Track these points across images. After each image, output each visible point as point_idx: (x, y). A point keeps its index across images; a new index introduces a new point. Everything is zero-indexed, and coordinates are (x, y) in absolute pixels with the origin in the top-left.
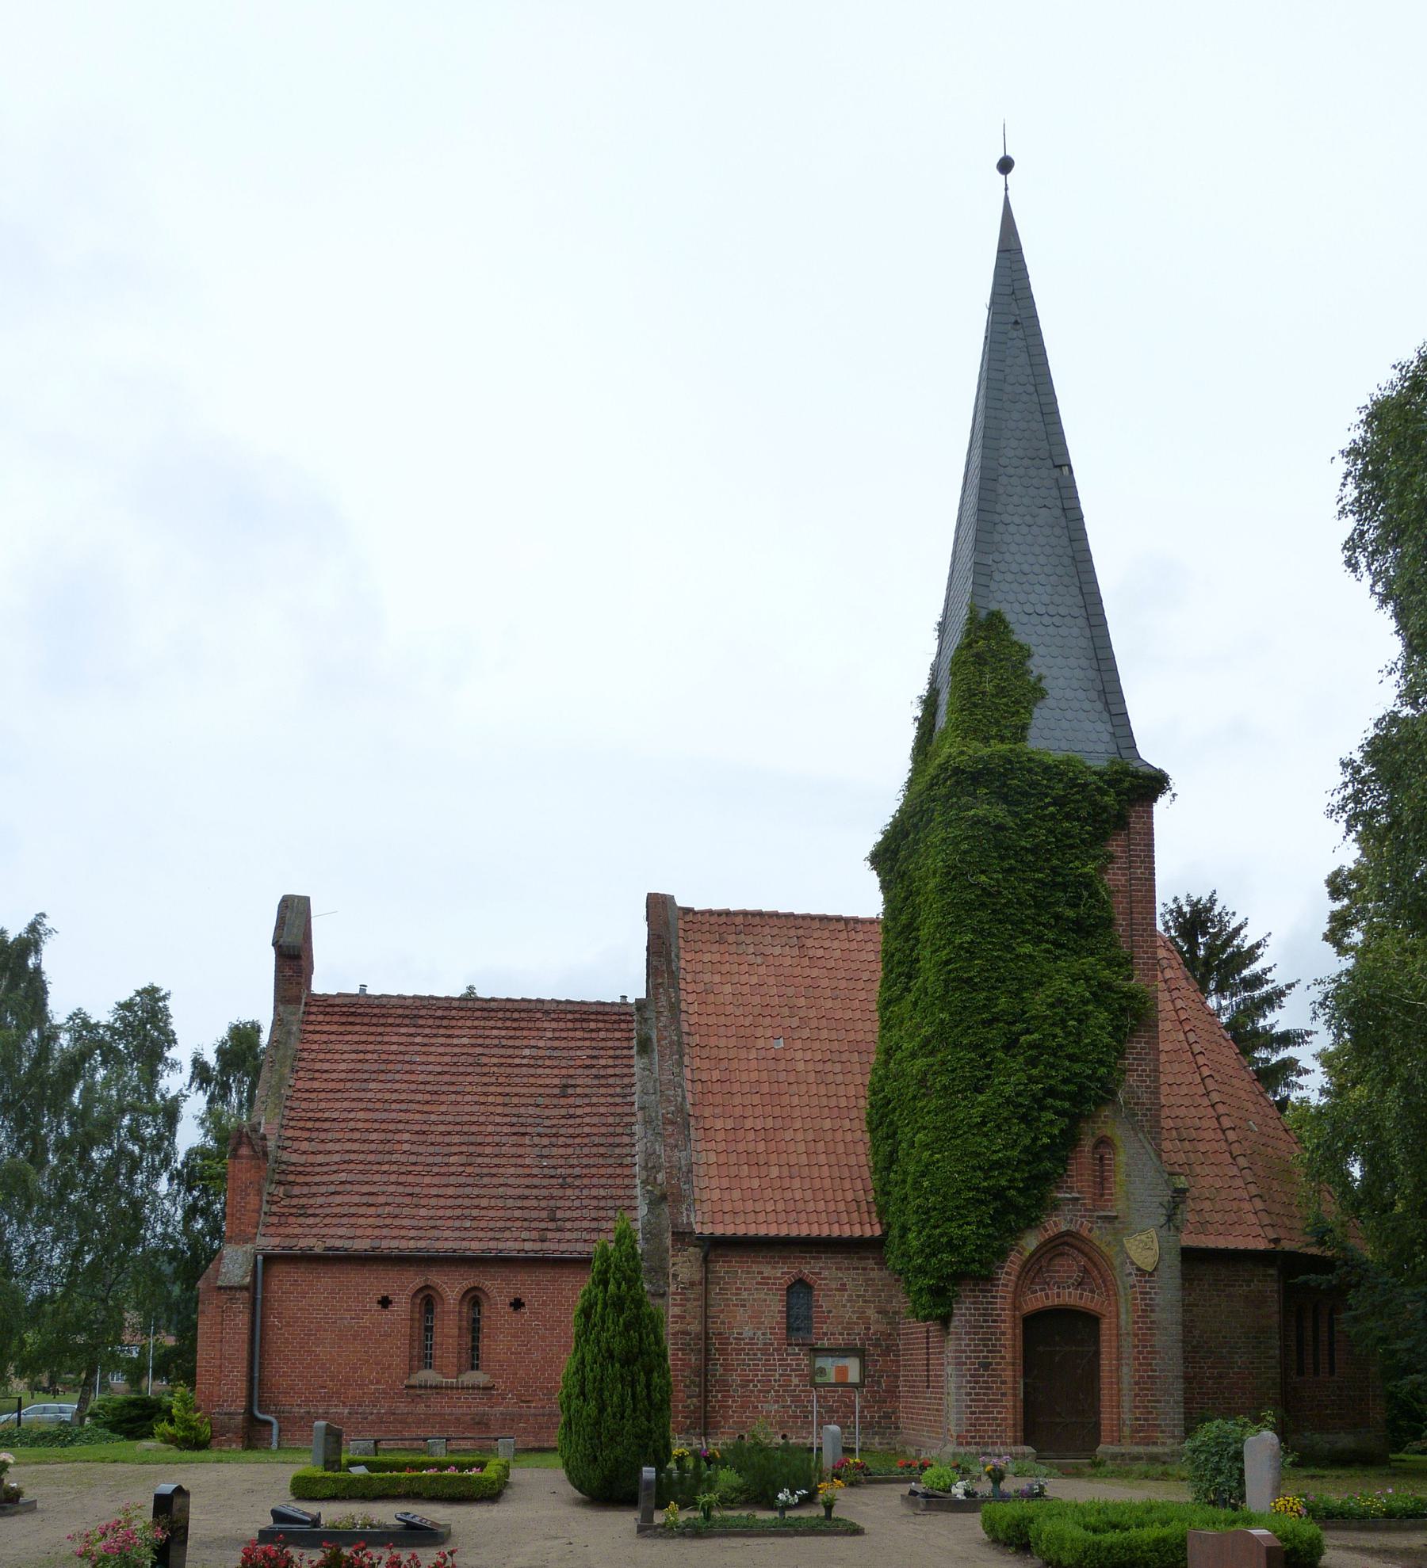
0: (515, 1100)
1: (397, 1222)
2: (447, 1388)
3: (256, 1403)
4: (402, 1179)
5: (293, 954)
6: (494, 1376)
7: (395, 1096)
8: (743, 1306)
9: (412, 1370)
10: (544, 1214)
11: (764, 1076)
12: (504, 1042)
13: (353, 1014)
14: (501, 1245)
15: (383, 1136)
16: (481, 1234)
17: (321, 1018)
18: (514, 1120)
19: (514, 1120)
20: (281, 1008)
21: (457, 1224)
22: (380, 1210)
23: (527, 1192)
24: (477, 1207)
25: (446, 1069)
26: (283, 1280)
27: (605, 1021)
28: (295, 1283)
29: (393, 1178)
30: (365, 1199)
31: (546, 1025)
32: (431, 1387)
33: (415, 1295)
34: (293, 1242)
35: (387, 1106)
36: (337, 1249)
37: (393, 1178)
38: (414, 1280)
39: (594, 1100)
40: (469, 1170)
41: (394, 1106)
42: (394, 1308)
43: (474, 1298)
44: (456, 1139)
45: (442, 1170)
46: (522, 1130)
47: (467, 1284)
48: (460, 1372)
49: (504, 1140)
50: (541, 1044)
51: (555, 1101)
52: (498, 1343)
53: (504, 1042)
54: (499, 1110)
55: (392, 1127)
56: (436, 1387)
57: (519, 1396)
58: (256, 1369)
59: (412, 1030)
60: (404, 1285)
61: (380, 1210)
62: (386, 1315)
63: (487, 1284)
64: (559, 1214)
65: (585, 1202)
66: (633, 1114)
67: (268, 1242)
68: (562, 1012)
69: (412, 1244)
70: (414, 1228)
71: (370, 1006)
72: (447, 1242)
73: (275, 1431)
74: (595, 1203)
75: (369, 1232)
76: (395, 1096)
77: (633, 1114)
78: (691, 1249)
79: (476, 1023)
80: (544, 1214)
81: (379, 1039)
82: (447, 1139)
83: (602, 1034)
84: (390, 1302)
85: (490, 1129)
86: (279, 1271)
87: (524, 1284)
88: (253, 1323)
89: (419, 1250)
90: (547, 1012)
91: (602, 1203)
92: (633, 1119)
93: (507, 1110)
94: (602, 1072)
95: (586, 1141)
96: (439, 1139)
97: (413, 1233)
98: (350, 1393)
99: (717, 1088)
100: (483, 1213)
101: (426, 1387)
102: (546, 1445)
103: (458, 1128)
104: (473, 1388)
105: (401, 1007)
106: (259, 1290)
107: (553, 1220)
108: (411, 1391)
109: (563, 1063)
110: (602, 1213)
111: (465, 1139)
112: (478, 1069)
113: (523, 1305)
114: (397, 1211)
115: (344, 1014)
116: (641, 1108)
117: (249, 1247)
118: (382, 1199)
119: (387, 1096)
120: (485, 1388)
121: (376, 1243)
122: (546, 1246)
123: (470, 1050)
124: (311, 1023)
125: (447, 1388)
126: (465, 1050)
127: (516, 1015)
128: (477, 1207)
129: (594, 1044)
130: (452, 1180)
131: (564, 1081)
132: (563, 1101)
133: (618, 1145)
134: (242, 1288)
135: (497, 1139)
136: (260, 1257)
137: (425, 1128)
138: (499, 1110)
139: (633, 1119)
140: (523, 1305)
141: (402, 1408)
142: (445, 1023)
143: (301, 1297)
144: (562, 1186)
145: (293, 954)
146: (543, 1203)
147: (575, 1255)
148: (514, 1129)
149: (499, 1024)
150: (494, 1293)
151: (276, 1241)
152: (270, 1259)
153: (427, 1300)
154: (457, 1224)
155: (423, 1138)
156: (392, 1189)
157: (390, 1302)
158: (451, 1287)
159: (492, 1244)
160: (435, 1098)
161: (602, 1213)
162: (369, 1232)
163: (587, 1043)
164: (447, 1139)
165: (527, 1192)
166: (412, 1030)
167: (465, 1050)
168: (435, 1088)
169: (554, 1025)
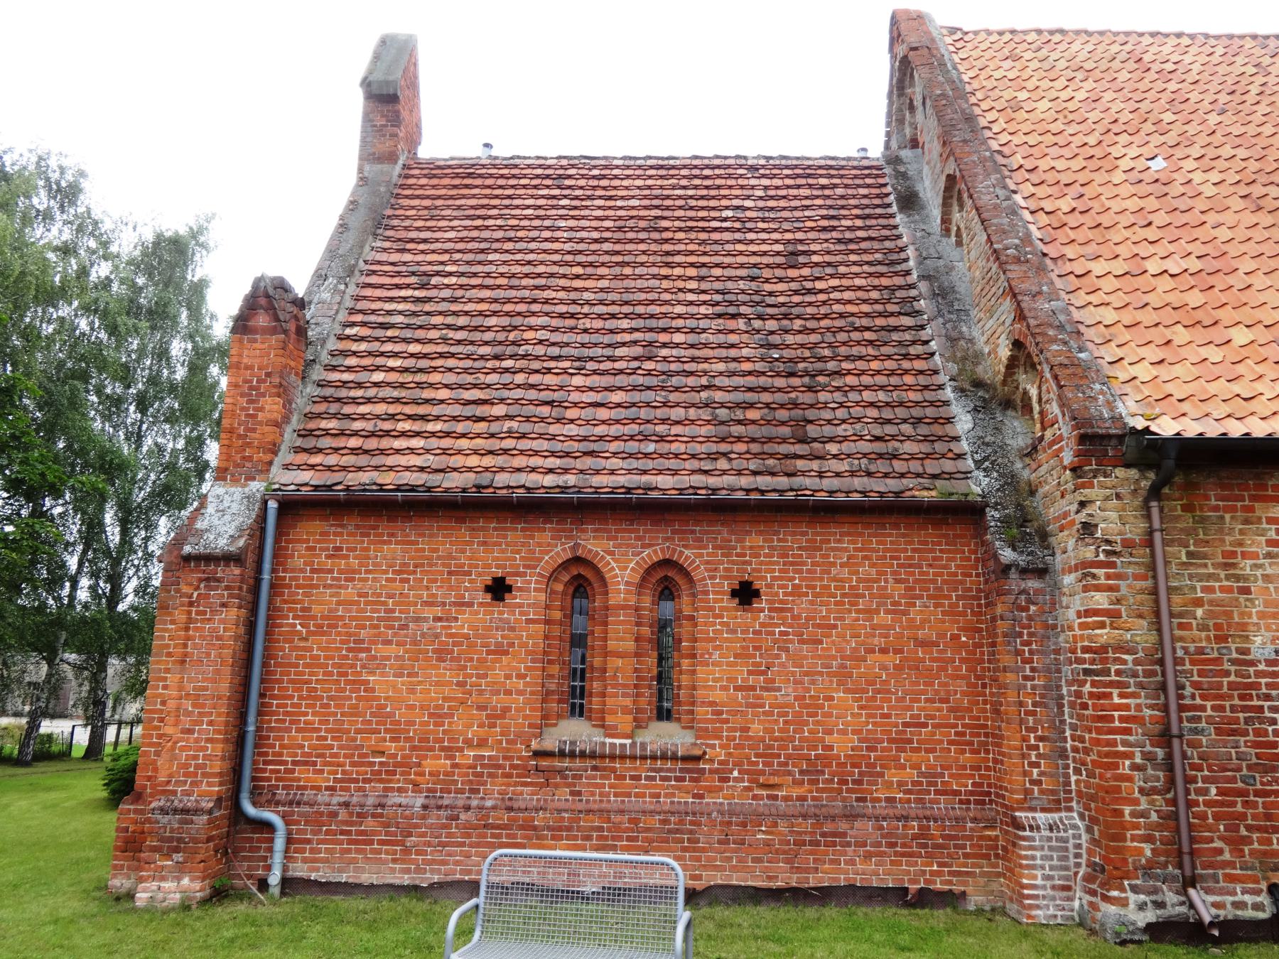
0: (717, 272)
1: (524, 444)
2: (613, 757)
3: (246, 784)
4: (534, 379)
5: (389, 101)
6: (702, 733)
7: (527, 269)
8: (1246, 591)
9: (547, 720)
10: (785, 431)
11: (1152, 203)
12: (693, 203)
13: (469, 175)
14: (712, 481)
15: (505, 321)
16: (673, 464)
17: (423, 181)
18: (718, 298)
19: (718, 298)
20: (367, 168)
21: (632, 446)
22: (495, 428)
23: (750, 397)
24: (664, 421)
25: (607, 235)
26: (312, 546)
27: (842, 177)
28: (337, 552)
29: (520, 378)
30: (468, 411)
31: (753, 182)
32: (583, 755)
33: (553, 576)
34: (338, 477)
35: (515, 282)
36: (413, 488)
37: (520, 378)
38: (551, 546)
39: (842, 269)
40: (649, 365)
41: (525, 282)
42: (516, 599)
43: (666, 580)
44: (625, 324)
45: (603, 366)
46: (732, 310)
47: (651, 555)
48: (639, 724)
49: (703, 324)
50: (748, 203)
51: (779, 273)
52: (714, 675)
53: (693, 203)
54: (693, 285)
55: (522, 308)
56: (593, 756)
57: (754, 775)
58: (251, 718)
59: (556, 192)
60: (534, 554)
61: (495, 428)
62: (501, 613)
63: (688, 555)
64: (812, 431)
65: (857, 411)
66: (911, 286)
67: (292, 477)
68: (775, 167)
69: (549, 480)
70: (553, 454)
71: (495, 166)
72: (612, 477)
73: (279, 843)
74: (873, 413)
75: (473, 461)
76: (527, 269)
77: (911, 286)
78: (1120, 472)
79: (650, 182)
80: (785, 431)
81: (507, 202)
82: (611, 324)
83: (839, 191)
84: (509, 589)
85: (679, 309)
86: (310, 531)
87: (759, 553)
88: (251, 626)
89: (564, 489)
90: (753, 168)
91: (887, 414)
92: (913, 293)
93: (704, 286)
94: (848, 235)
95: (840, 323)
96: (598, 324)
97: (552, 462)
98: (429, 765)
99: (1073, 220)
100: (676, 430)
101: (572, 755)
102: (813, 881)
103: (626, 309)
104: (664, 757)
105: (540, 166)
106: (267, 566)
107: (803, 441)
108: (544, 763)
109: (786, 226)
110: (890, 429)
111: (639, 323)
112: (656, 235)
113: (756, 594)
114: (526, 427)
115: (457, 176)
116: (922, 277)
117: (257, 486)
118: (499, 410)
119: (516, 269)
120: (685, 759)
121: (485, 479)
122: (797, 481)
123: (643, 213)
124: (410, 187)
125: (613, 757)
126: (634, 213)
127: (707, 172)
128: (664, 421)
129: (829, 202)
130: (621, 380)
131: (790, 248)
132: (792, 273)
133: (896, 329)
134: (227, 558)
135: (691, 323)
136: (273, 505)
137: (573, 309)
138: (693, 285)
139: (913, 293)
140: (756, 594)
141: (527, 795)
142: (604, 183)
143: (346, 580)
144: (810, 389)
145: (389, 101)
146: (782, 414)
147: (856, 497)
148: (718, 309)
149: (684, 182)
150: (700, 573)
151: (305, 476)
152: (293, 508)
153: (581, 581)
154: (632, 446)
155: (570, 323)
156: (518, 393)
157: (509, 589)
158: (623, 561)
159: (697, 480)
160: (590, 270)
161: (890, 429)
162: (473, 461)
163: (819, 202)
164: (611, 324)
165: (750, 397)
166: (556, 192)
167: (634, 213)
168: (590, 259)
169: (766, 182)
